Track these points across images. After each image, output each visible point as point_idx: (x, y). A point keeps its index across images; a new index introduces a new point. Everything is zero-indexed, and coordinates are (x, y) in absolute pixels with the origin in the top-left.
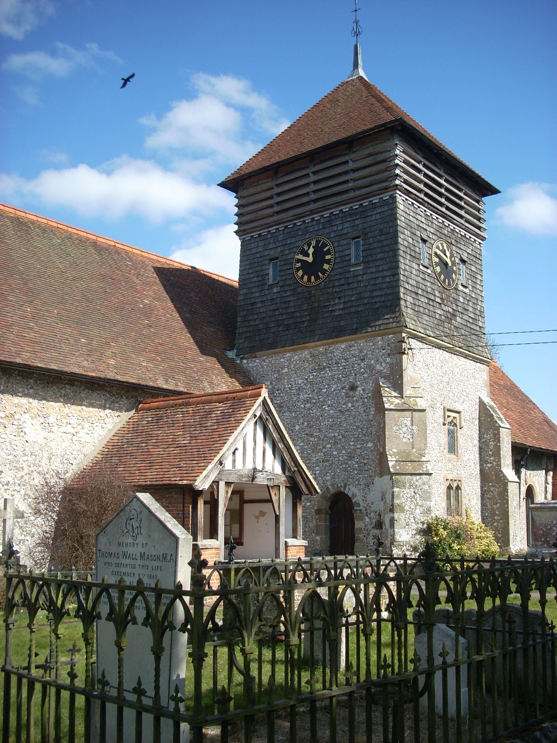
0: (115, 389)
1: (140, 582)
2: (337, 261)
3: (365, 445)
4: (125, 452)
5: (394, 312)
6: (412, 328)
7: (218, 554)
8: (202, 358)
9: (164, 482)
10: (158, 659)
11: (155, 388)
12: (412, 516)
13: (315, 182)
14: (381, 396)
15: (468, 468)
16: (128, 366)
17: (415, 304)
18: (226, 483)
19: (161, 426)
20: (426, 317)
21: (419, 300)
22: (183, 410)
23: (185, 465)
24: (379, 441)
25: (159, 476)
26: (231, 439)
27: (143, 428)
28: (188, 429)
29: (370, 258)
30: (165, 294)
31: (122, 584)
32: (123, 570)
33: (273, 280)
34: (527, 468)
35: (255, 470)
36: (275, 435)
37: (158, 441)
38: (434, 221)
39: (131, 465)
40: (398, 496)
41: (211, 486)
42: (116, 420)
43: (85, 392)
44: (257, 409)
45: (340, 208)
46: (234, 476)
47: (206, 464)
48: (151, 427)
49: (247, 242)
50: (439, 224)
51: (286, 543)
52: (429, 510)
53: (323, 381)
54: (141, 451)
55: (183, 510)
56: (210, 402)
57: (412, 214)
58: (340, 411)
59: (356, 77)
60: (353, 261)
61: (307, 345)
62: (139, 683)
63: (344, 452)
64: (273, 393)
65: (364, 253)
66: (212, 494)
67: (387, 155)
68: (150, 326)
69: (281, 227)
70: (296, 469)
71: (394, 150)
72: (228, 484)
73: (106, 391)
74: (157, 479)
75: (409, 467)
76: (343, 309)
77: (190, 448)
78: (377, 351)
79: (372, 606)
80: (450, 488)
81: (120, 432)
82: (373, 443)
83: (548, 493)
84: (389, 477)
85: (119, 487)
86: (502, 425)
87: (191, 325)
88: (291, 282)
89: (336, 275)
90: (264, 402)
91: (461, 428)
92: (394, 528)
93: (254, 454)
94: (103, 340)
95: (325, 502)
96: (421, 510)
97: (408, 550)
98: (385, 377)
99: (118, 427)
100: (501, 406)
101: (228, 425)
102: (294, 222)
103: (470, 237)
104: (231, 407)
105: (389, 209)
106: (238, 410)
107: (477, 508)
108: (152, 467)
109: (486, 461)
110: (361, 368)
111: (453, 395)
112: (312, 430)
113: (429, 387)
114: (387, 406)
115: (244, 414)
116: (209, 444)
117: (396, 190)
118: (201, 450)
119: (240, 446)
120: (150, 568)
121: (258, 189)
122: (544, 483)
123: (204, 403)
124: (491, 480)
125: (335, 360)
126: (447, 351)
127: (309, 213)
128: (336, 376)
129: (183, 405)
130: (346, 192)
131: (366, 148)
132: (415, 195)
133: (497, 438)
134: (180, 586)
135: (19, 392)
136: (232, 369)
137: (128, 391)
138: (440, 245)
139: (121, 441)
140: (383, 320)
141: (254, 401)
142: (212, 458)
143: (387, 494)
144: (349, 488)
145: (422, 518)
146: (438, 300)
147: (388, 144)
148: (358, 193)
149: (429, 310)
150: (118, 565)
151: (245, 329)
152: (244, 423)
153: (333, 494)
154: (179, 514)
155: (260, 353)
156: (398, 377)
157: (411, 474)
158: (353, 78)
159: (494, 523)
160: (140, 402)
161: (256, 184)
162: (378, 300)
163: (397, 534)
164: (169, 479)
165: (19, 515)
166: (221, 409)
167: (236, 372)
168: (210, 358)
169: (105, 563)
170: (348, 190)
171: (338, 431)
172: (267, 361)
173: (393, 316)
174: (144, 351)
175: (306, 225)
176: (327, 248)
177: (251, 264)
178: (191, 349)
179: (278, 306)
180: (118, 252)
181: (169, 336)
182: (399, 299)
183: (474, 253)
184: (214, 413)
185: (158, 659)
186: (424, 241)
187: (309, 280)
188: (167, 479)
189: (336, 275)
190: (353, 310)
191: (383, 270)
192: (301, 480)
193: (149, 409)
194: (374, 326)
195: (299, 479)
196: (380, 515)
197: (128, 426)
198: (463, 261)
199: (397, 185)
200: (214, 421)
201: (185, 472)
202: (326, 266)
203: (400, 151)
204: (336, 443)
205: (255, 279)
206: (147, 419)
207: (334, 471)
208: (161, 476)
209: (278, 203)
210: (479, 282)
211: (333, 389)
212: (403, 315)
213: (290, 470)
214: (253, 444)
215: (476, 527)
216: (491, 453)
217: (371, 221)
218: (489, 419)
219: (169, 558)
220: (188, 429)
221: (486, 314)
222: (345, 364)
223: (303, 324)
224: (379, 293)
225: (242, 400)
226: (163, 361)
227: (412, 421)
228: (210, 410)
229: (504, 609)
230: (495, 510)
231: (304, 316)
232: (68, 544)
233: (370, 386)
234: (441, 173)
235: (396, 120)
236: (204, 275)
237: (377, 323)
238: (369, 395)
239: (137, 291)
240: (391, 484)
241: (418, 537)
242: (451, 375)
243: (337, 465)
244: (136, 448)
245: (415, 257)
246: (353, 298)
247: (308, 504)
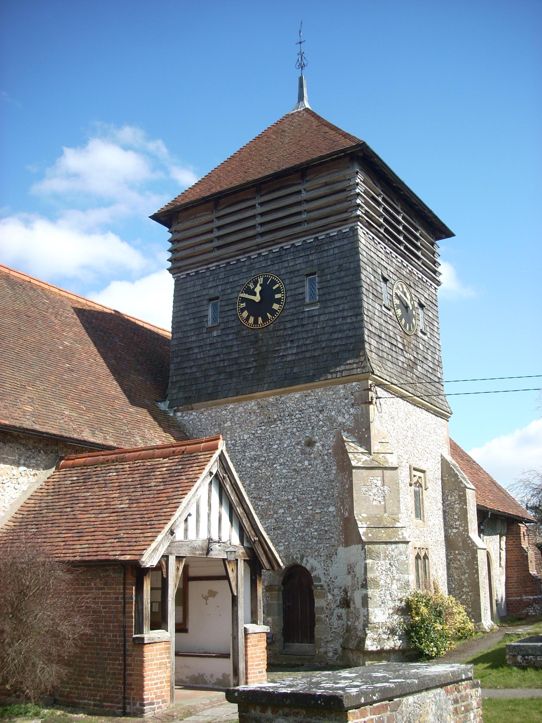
0: (31, 442)
2: (288, 301)
3: (325, 509)
4: (45, 519)
5: (358, 357)
6: (379, 375)
7: (168, 648)
8: (132, 409)
9: (99, 557)
11: (81, 441)
12: (388, 592)
13: (262, 214)
14: (345, 452)
15: (434, 534)
16: (48, 414)
17: (379, 349)
18: (176, 557)
19: (90, 487)
20: (389, 364)
21: (382, 344)
22: (117, 467)
23: (125, 536)
25: (91, 550)
26: (184, 501)
27: (67, 489)
28: (125, 491)
29: (327, 297)
30: (87, 337)
33: (212, 323)
35: (210, 541)
36: (233, 497)
37: (87, 505)
38: (394, 260)
39: (53, 536)
40: (371, 569)
41: (160, 562)
42: (32, 479)
44: (213, 465)
45: (292, 242)
46: (186, 548)
47: (154, 534)
48: (77, 488)
49: (182, 281)
50: (398, 264)
51: (245, 629)
53: (273, 436)
54: (66, 517)
55: (124, 593)
56: (152, 457)
57: (372, 249)
58: (295, 470)
59: (302, 109)
60: (307, 300)
61: (254, 395)
63: (300, 517)
65: (321, 290)
67: (346, 184)
68: (72, 370)
69: (222, 264)
70: (256, 539)
71: (354, 177)
73: (21, 444)
74: (90, 554)
75: (383, 535)
76: (296, 354)
77: (130, 513)
78: (339, 401)
80: (418, 557)
81: (37, 494)
82: (336, 507)
83: (502, 560)
84: (360, 546)
86: (468, 486)
87: (118, 372)
88: (234, 324)
89: (287, 316)
90: (222, 457)
91: (426, 490)
92: (368, 608)
93: (209, 520)
94: (18, 383)
95: (277, 577)
96: (399, 585)
97: (384, 633)
98: (348, 431)
99: (35, 489)
101: (178, 485)
102: (237, 258)
103: (427, 281)
104: (180, 463)
105: (349, 243)
106: (189, 466)
107: (443, 580)
108: (81, 538)
109: (452, 526)
110: (320, 420)
111: (417, 452)
112: (261, 493)
113: (395, 442)
114: (354, 463)
115: (198, 472)
117: (357, 221)
118: (145, 516)
119: (193, 512)
121: (196, 222)
122: (498, 549)
123: (144, 458)
125: (288, 411)
126: (410, 403)
127: (255, 247)
128: (289, 430)
129: (117, 461)
130: (299, 224)
131: (322, 177)
132: (376, 229)
133: (463, 500)
136: (166, 423)
137: (47, 445)
138: (400, 286)
139: (38, 505)
140: (345, 365)
141: (209, 456)
142: (161, 526)
144: (307, 560)
145: (399, 594)
146: (400, 346)
147: (348, 172)
148: (312, 225)
149: (392, 356)
151: (179, 378)
152: (199, 481)
154: (117, 598)
155: (197, 404)
156: (364, 430)
157: (386, 543)
158: (299, 110)
159: (462, 596)
160: (62, 459)
161: (193, 217)
162: (338, 343)
163: (372, 614)
164: (105, 553)
166: (167, 465)
167: (169, 426)
168: (140, 409)
170: (301, 222)
172: (205, 413)
173: (357, 361)
174: (66, 397)
175: (252, 261)
176: (277, 285)
177: (187, 304)
178: (118, 398)
179: (219, 351)
180: (33, 288)
181: (94, 383)
182: (363, 341)
183: (430, 299)
184: (158, 470)
186: (385, 280)
187: (256, 322)
188: (103, 553)
189: (287, 316)
190: (308, 354)
191: (343, 310)
192: (262, 552)
193: (73, 466)
194: (334, 372)
195: (260, 551)
196: (346, 591)
197: (46, 487)
198: (422, 306)
199: (359, 216)
200: (159, 480)
201: (127, 544)
202: (276, 306)
203: (361, 181)
204: (290, 507)
205: (192, 322)
206: (71, 479)
207: (288, 541)
208: (95, 550)
209: (219, 238)
210: (436, 330)
211: (286, 445)
212: (369, 360)
213: (249, 540)
214: (208, 508)
216: (456, 517)
217: (328, 256)
218: (453, 479)
220: (125, 491)
221: (443, 364)
222: (300, 416)
223: (249, 371)
224: (340, 335)
225: (195, 454)
226: (88, 410)
227: (383, 480)
228: (152, 467)
230: (463, 582)
231: (250, 362)
233: (331, 440)
234: (399, 209)
235: (358, 145)
236: (128, 320)
237: (338, 369)
238: (330, 451)
239: (57, 332)
240: (363, 554)
241: (396, 617)
242: (415, 429)
243: (292, 533)
244: (59, 514)
245: (377, 297)
246: (308, 342)
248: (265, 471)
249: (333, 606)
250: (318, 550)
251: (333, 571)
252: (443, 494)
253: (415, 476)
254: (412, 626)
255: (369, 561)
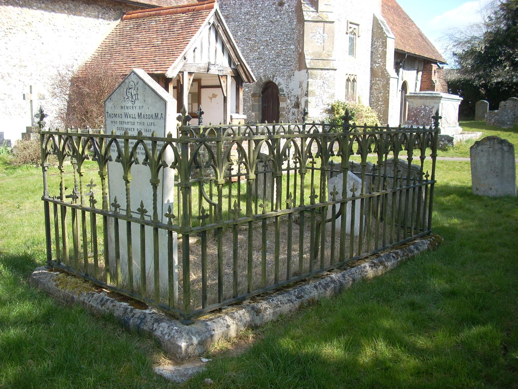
1: (140, 133)
3: (288, 47)
10: (155, 187)
14: (302, 11)
24: (299, 44)
26: (192, 40)
28: (160, 33)
31: (127, 135)
32: (125, 126)
34: (404, 68)
35: (209, 64)
36: (224, 38)
40: (311, 85)
41: (178, 75)
43: (83, 6)
44: (211, 18)
46: (194, 67)
47: (174, 59)
51: (231, 116)
52: (333, 95)
56: (176, 13)
58: (271, 21)
62: (142, 205)
64: (222, 7)
66: (178, 81)
70: (239, 63)
72: (190, 73)
73: (99, 5)
75: (320, 64)
79: (306, 154)
80: (348, 80)
84: (305, 70)
85: (112, 76)
90: (216, 13)
93: (209, 52)
100: (389, 21)
114: (306, 18)
116: (175, 46)
120: (146, 124)
124: (377, 75)
134: (170, 135)
135: (34, 6)
137: (115, 5)
143: (304, 83)
150: (121, 123)
152: (201, 28)
153: (264, 83)
157: (322, 69)
160: (124, 14)
165: (41, 97)
169: (112, 122)
171: (269, 36)
185: (155, 187)
195: (241, 71)
196: (298, 98)
204: (267, 45)
213: (234, 64)
214: (208, 44)
215: (365, 109)
216: (379, 56)
219: (160, 116)
220: (160, 33)
229: (396, 160)
232: (77, 117)
233: (294, 3)
241: (324, 114)
247: (247, 89)
248: (253, 22)
249: (290, 107)
250: (283, 73)
251: (292, 85)
252: (372, 41)
253: (350, 28)
254: (334, 120)
255: (310, 80)
